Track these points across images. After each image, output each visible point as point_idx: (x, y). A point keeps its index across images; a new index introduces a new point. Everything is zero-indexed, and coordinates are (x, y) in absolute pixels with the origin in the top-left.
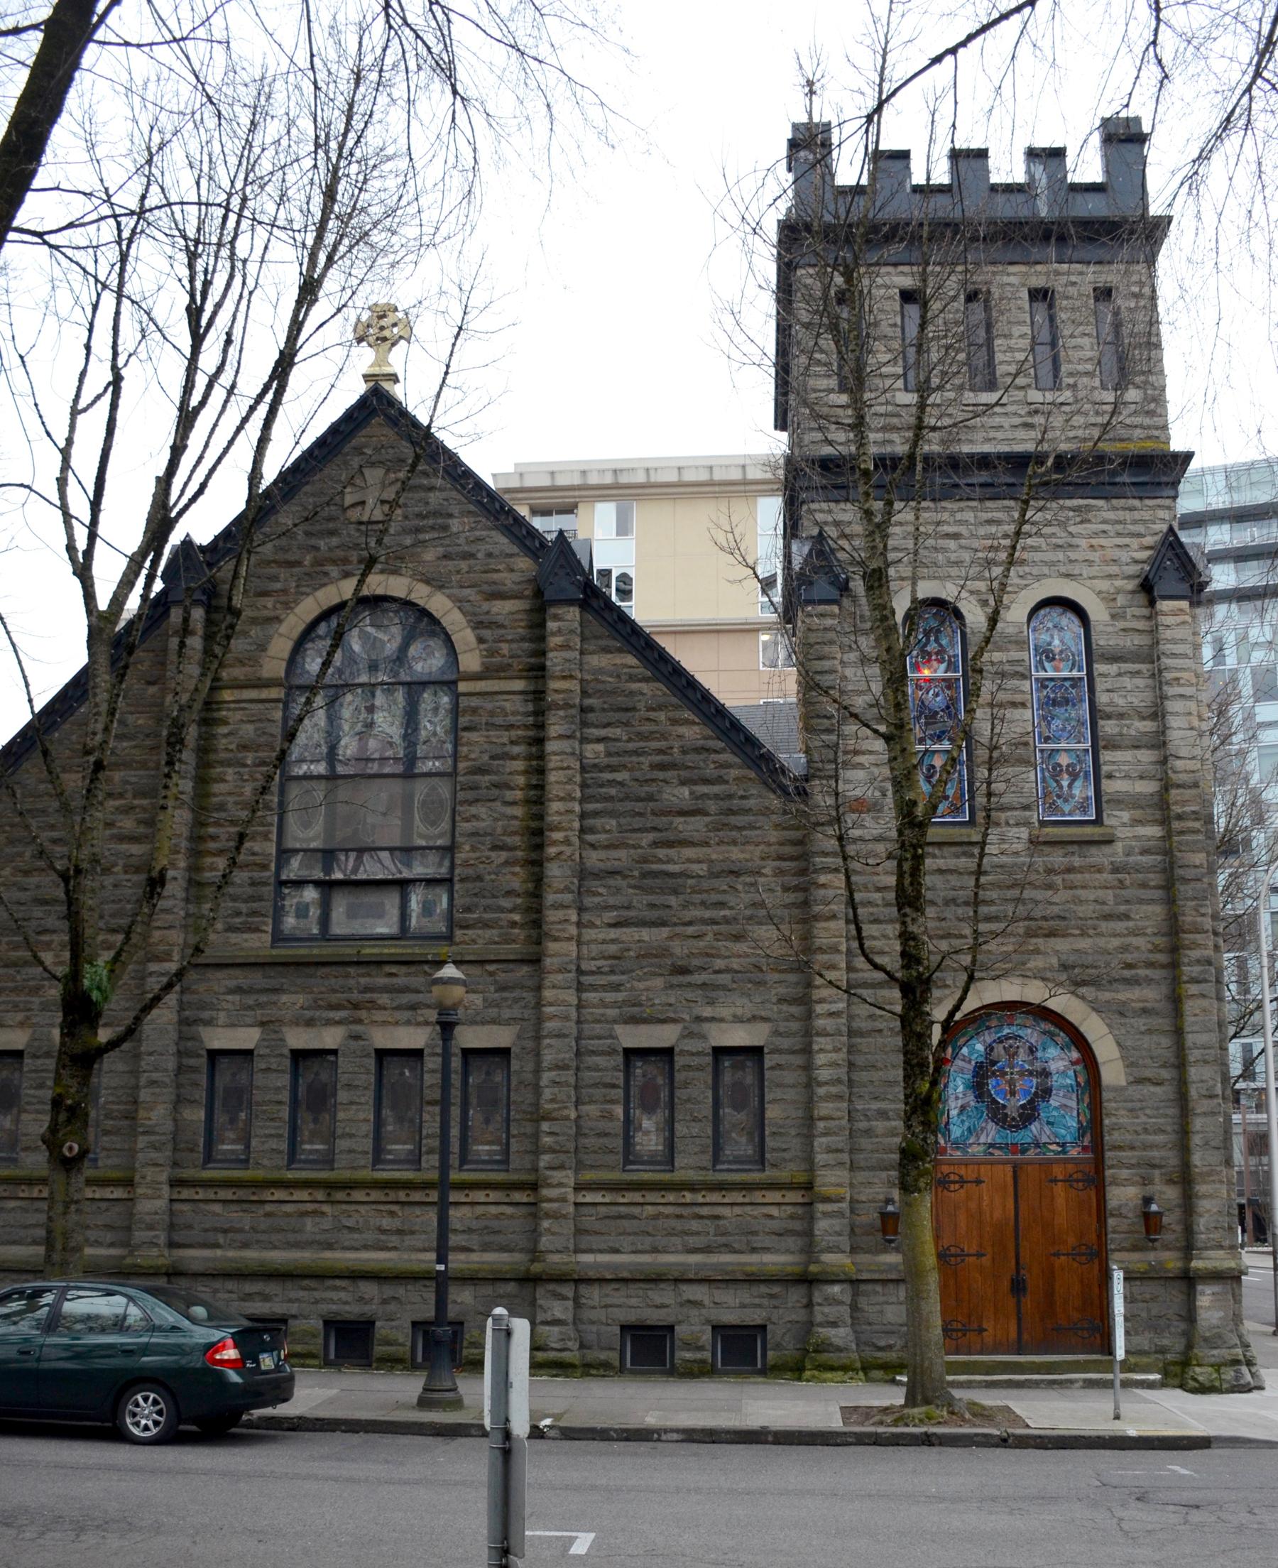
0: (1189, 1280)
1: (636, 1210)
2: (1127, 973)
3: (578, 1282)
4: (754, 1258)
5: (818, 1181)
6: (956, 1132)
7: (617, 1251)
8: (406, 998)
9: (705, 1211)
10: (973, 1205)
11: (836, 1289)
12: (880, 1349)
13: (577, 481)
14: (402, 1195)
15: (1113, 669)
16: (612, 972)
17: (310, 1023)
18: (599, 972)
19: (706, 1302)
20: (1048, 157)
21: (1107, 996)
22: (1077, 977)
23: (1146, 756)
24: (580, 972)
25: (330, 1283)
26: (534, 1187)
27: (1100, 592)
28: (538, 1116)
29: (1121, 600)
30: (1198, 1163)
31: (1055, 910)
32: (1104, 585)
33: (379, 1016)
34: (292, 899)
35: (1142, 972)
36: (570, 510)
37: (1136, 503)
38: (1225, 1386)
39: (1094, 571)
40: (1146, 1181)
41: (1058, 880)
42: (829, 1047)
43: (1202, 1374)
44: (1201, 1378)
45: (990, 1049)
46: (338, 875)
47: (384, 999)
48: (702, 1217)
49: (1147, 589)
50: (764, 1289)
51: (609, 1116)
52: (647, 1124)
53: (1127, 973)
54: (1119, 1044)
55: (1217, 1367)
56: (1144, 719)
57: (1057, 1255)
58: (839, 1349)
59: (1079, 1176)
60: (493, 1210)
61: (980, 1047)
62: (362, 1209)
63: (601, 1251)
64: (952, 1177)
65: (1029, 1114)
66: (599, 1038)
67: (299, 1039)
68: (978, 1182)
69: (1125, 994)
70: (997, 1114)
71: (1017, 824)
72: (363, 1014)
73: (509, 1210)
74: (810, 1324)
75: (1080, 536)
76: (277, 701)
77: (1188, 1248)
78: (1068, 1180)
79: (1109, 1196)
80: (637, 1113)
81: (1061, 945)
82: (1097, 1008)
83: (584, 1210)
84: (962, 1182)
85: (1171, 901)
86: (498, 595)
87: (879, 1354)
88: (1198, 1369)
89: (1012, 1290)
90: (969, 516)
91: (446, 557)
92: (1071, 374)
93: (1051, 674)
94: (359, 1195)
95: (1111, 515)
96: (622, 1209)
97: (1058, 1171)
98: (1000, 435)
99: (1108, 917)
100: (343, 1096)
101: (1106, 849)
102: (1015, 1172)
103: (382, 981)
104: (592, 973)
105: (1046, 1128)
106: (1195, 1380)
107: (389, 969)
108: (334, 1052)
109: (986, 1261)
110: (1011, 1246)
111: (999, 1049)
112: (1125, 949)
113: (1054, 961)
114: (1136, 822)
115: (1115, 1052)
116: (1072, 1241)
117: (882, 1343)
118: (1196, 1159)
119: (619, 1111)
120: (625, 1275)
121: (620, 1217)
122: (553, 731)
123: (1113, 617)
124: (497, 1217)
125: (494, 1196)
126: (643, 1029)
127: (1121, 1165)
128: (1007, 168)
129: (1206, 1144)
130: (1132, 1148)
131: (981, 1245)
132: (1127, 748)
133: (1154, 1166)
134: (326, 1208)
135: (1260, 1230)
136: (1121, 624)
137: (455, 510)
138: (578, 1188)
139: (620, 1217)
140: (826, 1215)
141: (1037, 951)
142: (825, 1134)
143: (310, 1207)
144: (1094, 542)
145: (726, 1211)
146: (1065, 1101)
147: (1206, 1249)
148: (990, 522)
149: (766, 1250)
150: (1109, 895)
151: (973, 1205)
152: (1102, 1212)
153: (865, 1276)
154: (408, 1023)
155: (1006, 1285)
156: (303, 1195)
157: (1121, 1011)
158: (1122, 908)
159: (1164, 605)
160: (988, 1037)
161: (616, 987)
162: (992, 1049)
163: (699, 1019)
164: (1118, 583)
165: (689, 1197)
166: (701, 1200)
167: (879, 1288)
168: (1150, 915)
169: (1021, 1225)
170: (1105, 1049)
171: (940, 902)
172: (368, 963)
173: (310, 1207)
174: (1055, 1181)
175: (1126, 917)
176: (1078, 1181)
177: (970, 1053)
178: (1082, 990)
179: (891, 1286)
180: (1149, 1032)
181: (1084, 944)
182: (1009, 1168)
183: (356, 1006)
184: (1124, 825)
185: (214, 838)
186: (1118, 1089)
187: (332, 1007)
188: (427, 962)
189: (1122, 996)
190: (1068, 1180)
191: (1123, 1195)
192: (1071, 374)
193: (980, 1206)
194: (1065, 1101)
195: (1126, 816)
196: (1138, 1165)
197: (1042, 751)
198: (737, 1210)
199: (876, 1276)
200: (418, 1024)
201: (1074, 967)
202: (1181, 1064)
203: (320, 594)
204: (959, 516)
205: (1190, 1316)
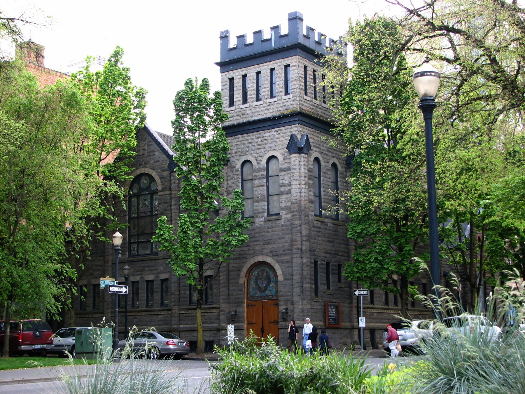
1: (190, 315)
2: (284, 252)
3: (180, 331)
4: (211, 325)
5: (221, 306)
7: (187, 324)
8: (150, 268)
14: (150, 313)
17: (134, 275)
20: (276, 28)
21: (279, 259)
31: (269, 238)
33: (146, 273)
35: (287, 252)
39: (280, 148)
41: (270, 230)
45: (258, 273)
46: (140, 240)
47: (146, 269)
50: (213, 332)
51: (185, 293)
52: (195, 295)
60: (165, 316)
61: (256, 273)
65: (266, 289)
70: (259, 288)
72: (143, 273)
73: (168, 316)
80: (192, 292)
81: (270, 246)
82: (278, 262)
86: (163, 171)
90: (254, 137)
91: (155, 162)
92: (278, 93)
94: (143, 313)
95: (285, 131)
98: (261, 113)
99: (280, 239)
101: (280, 221)
103: (146, 264)
108: (138, 281)
111: (260, 273)
112: (283, 246)
114: (287, 214)
119: (188, 292)
120: (188, 329)
121: (188, 316)
122: (173, 204)
124: (166, 317)
125: (165, 312)
127: (281, 301)
128: (267, 34)
133: (288, 301)
136: (286, 161)
137: (156, 150)
138: (180, 310)
139: (188, 316)
140: (222, 314)
141: (265, 249)
145: (206, 314)
148: (258, 138)
149: (214, 323)
150: (280, 233)
154: (151, 274)
158: (283, 236)
160: (258, 270)
180: (288, 267)
181: (275, 246)
183: (142, 271)
186: (281, 282)
187: (138, 271)
189: (282, 258)
192: (278, 93)
195: (284, 212)
196: (285, 301)
198: (208, 314)
204: (252, 137)
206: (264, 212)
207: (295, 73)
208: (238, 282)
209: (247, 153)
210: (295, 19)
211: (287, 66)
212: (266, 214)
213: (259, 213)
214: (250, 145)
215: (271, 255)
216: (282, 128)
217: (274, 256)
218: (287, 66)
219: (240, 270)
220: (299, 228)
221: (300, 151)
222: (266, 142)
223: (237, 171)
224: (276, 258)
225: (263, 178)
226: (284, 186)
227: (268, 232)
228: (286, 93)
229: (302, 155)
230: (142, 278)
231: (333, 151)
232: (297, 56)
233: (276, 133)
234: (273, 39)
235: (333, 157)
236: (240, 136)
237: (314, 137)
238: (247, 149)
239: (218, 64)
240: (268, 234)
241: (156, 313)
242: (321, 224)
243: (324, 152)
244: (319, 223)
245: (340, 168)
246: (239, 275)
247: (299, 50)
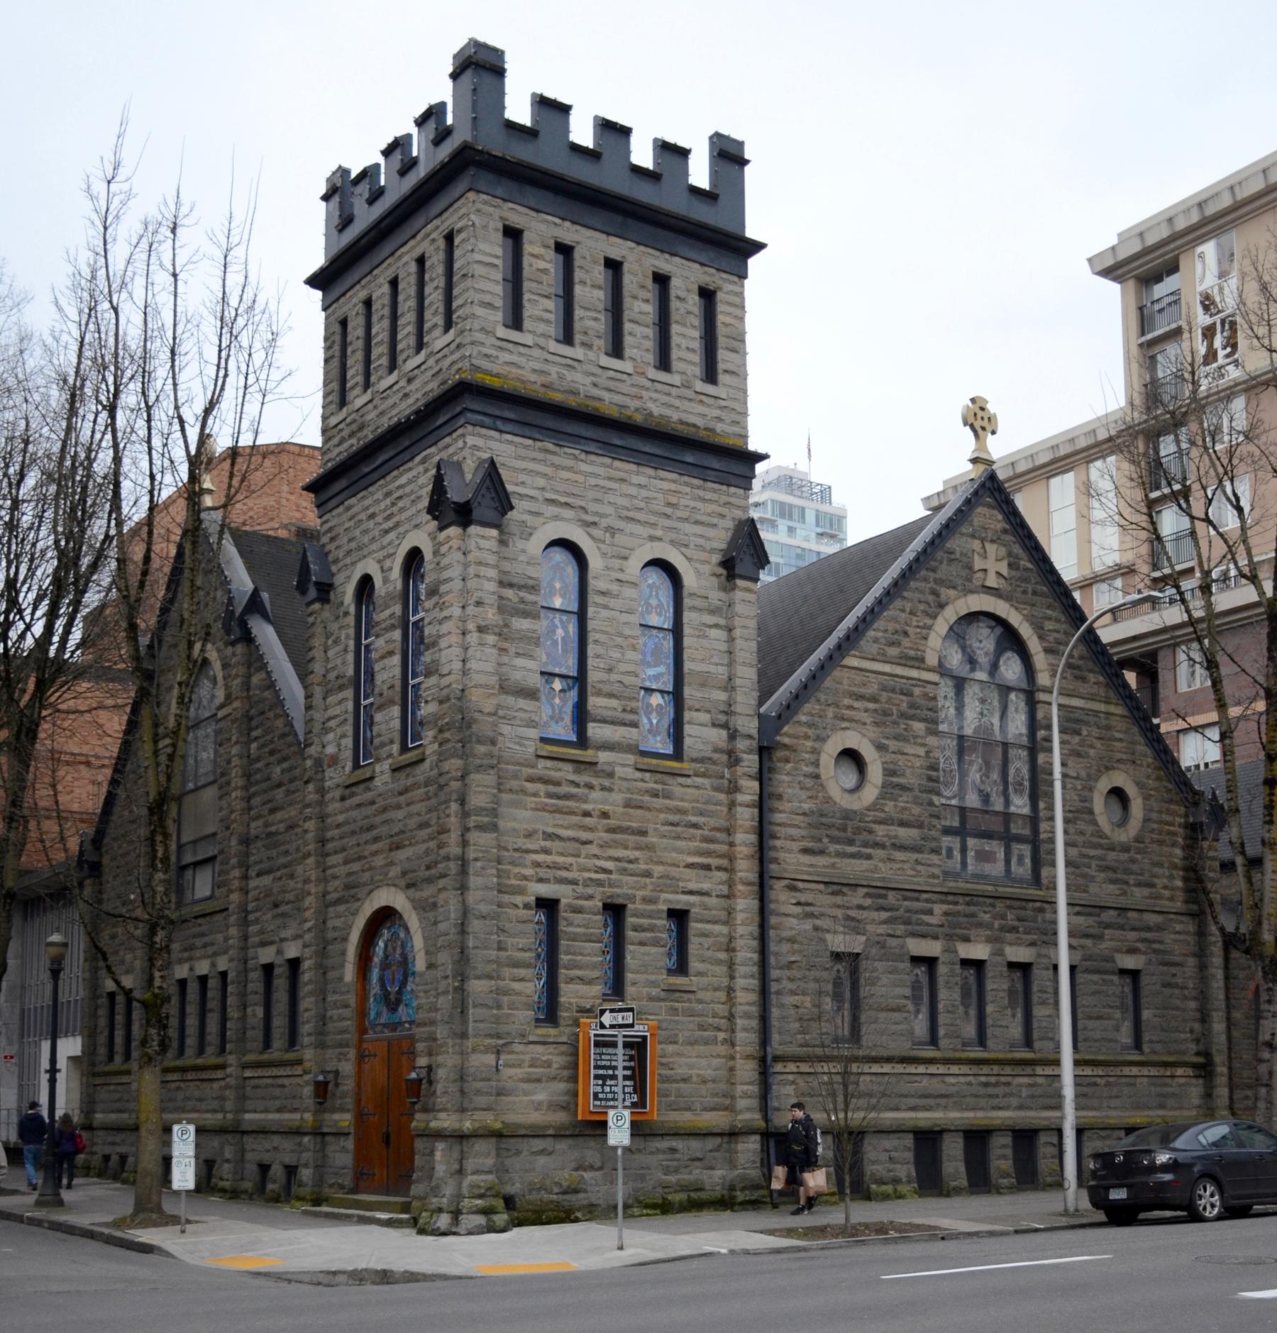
6: (372, 1014)
11: (306, 1139)
13: (1164, 233)
21: (418, 895)
36: (1173, 268)
37: (447, 440)
41: (402, 798)
145: (286, 1081)
163: (282, 940)
206: (392, 742)
207: (483, 255)
208: (341, 979)
209: (365, 551)
210: (480, 66)
211: (449, 238)
212: (396, 748)
214: (371, 524)
215: (402, 883)
216: (433, 450)
217: (409, 886)
218: (449, 238)
219: (345, 939)
220: (455, 785)
221: (464, 515)
222: (400, 504)
223: (346, 614)
225: (393, 627)
227: (399, 807)
228: (448, 325)
229: (473, 529)
230: (191, 969)
231: (652, 519)
232: (471, 195)
233: (421, 468)
234: (422, 158)
235: (652, 538)
236: (353, 501)
237: (549, 470)
238: (366, 539)
239: (314, 281)
240: (400, 814)
242: (577, 772)
243: (604, 523)
244: (568, 767)
245: (689, 579)
246: (344, 953)
247: (484, 179)
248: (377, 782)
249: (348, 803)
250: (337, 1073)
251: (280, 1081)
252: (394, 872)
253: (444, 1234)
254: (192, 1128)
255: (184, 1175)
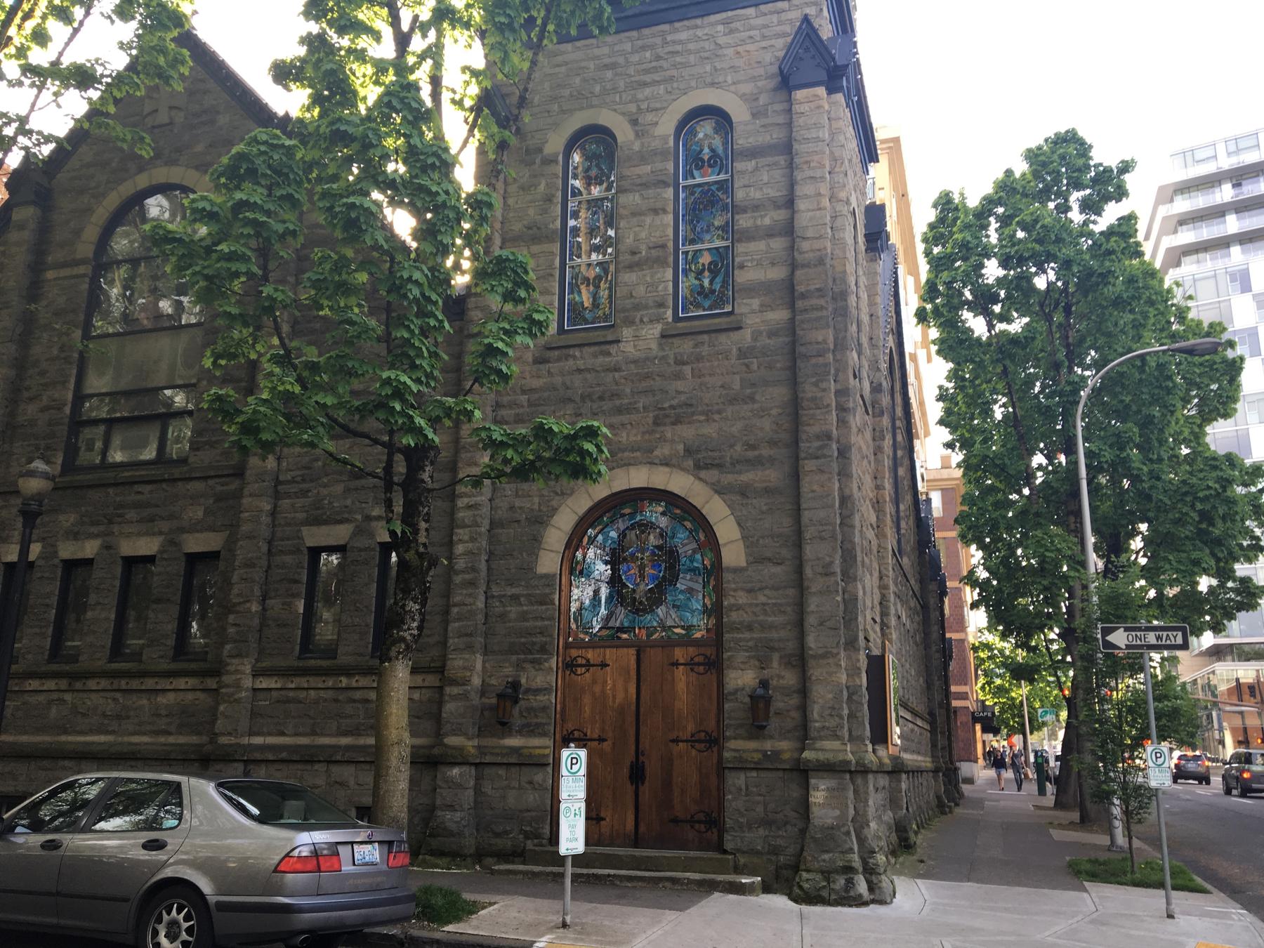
0: (803, 773)
1: (302, 695)
2: (751, 454)
9: (358, 695)
10: (597, 689)
12: (497, 835)
14: (123, 684)
15: (750, 165)
16: (304, 480)
18: (293, 481)
19: (352, 783)
22: (699, 460)
23: (778, 244)
24: (278, 482)
25: (61, 763)
26: (216, 672)
27: (744, 94)
28: (228, 609)
29: (763, 99)
30: (812, 645)
32: (747, 88)
34: (87, 433)
38: (833, 897)
40: (763, 663)
42: (466, 538)
43: (808, 879)
44: (806, 886)
45: (623, 535)
48: (354, 701)
49: (786, 82)
52: (326, 615)
53: (751, 454)
54: (739, 524)
55: (827, 874)
56: (779, 208)
57: (676, 741)
58: (452, 834)
59: (701, 659)
61: (613, 534)
62: (93, 696)
63: (270, 734)
64: (580, 661)
66: (288, 539)
67: (67, 551)
68: (604, 665)
69: (747, 477)
71: (651, 321)
74: (432, 809)
75: (729, 46)
76: (84, 275)
77: (803, 733)
78: (691, 664)
79: (726, 680)
81: (687, 432)
82: (720, 490)
83: (261, 695)
84: (588, 665)
85: (794, 382)
87: (498, 841)
88: (805, 875)
89: (630, 777)
93: (699, 180)
94: (92, 684)
96: (291, 694)
97: (679, 654)
99: (733, 401)
100: (93, 598)
101: (735, 336)
102: (638, 655)
104: (288, 482)
105: (672, 612)
106: (801, 887)
107: (137, 488)
109: (607, 746)
110: (632, 732)
111: (632, 535)
113: (681, 447)
114: (764, 308)
115: (736, 533)
116: (691, 727)
117: (500, 829)
118: (811, 641)
123: (754, 115)
126: (324, 529)
129: (821, 624)
130: (750, 628)
131: (603, 730)
132: (761, 238)
134: (68, 697)
135: (1246, 287)
140: (454, 698)
141: (663, 439)
142: (459, 620)
143: (55, 696)
144: (740, 49)
146: (691, 584)
147: (821, 738)
151: (597, 689)
152: (721, 697)
153: (488, 759)
155: (626, 771)
156: (50, 684)
157: (744, 492)
159: (799, 95)
161: (305, 493)
162: (625, 536)
164: (760, 84)
165: (344, 681)
166: (354, 684)
167: (502, 772)
168: (778, 394)
169: (642, 710)
170: (727, 530)
171: (578, 399)
172: (122, 483)
173: (55, 696)
174: (676, 664)
175: (752, 399)
176: (699, 664)
177: (605, 540)
178: (703, 474)
179: (514, 770)
182: (633, 651)
184: (753, 312)
185: (28, 389)
186: (736, 570)
188: (164, 480)
190: (691, 664)
191: (741, 678)
193: (603, 691)
194: (691, 584)
195: (755, 303)
197: (686, 253)
199: (499, 760)
200: (154, 534)
201: (698, 451)
202: (798, 541)
203: (121, 188)
205: (804, 807)
213: (637, 307)
217: (698, 466)
224: (712, 475)
226: (756, 208)
230: (108, 547)
241: (150, 683)
248: (628, 348)
249: (554, 367)
250: (515, 685)
251: (358, 695)
252: (663, 451)
253: (866, 904)
254: (583, 754)
255: (572, 836)
